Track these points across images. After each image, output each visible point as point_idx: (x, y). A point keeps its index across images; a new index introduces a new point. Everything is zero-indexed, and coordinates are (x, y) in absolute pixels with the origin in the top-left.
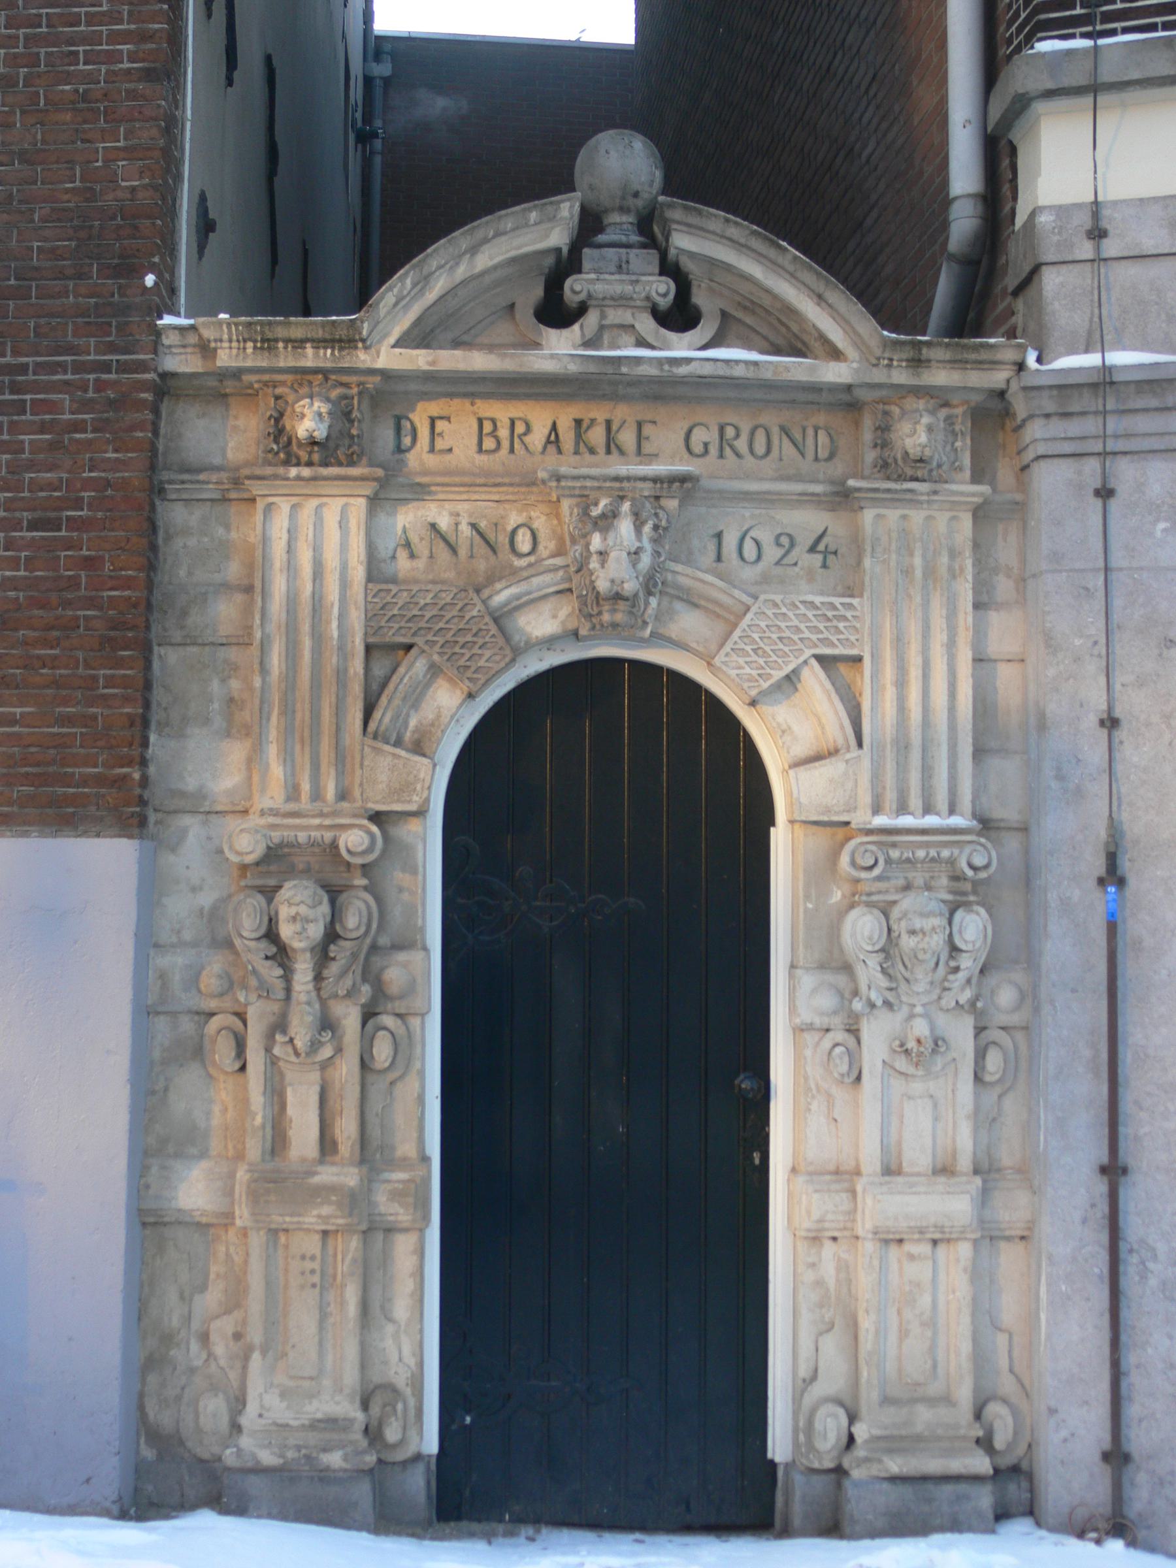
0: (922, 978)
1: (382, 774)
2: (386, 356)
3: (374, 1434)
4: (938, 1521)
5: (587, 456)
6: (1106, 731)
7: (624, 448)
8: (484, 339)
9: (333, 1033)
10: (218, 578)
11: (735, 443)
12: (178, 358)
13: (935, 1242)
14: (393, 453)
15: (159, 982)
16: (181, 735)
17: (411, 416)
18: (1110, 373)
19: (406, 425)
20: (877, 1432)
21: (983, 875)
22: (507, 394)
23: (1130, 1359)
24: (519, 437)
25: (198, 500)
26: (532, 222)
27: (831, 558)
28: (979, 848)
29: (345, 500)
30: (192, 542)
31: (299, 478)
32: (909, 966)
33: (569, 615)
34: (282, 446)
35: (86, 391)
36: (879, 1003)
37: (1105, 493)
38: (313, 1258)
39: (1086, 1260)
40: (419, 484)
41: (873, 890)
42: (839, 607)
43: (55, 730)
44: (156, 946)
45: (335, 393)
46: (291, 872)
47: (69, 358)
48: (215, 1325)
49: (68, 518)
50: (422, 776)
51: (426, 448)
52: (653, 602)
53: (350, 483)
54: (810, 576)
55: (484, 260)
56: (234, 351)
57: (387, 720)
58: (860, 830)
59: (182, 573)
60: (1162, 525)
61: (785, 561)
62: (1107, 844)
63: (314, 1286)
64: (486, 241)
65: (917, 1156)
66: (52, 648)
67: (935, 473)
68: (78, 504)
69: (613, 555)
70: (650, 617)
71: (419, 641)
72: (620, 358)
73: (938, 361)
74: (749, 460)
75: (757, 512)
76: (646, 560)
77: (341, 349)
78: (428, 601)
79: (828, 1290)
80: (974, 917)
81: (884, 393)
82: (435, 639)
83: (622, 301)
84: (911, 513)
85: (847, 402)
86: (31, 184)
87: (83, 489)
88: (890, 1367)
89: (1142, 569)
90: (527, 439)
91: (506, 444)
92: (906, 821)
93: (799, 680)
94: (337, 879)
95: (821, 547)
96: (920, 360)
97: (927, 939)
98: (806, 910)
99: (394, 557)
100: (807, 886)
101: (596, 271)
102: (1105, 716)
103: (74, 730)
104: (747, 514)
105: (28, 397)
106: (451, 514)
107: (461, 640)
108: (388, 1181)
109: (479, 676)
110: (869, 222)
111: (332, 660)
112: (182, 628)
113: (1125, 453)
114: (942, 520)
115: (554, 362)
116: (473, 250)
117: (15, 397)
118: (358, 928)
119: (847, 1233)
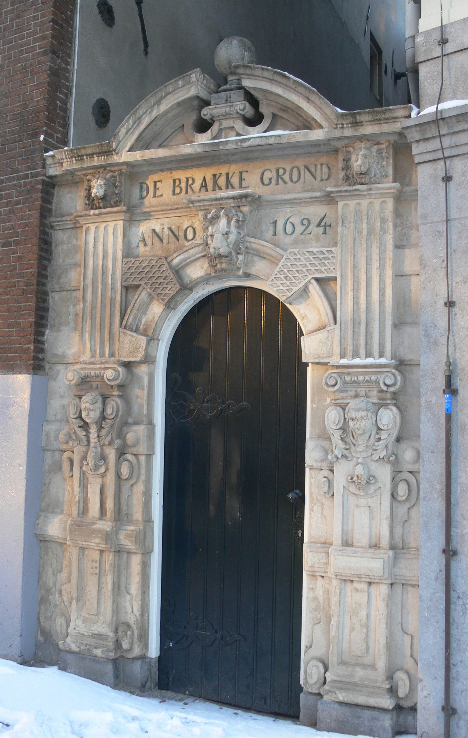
0: (361, 444)
1: (131, 345)
2: (125, 156)
3: (118, 643)
4: (363, 729)
5: (217, 191)
6: (447, 308)
7: (234, 185)
8: (172, 143)
9: (104, 461)
10: (72, 261)
11: (283, 177)
12: (54, 169)
13: (370, 583)
14: (139, 199)
15: (46, 437)
16: (59, 330)
17: (147, 182)
18: (441, 114)
19: (145, 186)
20: (335, 678)
22: (184, 167)
25: (67, 229)
26: (180, 86)
27: (328, 228)
28: (389, 374)
29: (115, 222)
30: (65, 247)
31: (94, 215)
32: (355, 437)
34: (92, 202)
35: (21, 187)
36: (339, 456)
38: (96, 562)
39: (437, 601)
40: (145, 212)
41: (340, 397)
42: (325, 252)
43: (8, 330)
44: (48, 421)
45: (108, 176)
46: (90, 389)
47: (15, 175)
48: (64, 587)
50: (142, 345)
51: (152, 196)
53: (114, 214)
54: (317, 239)
55: (164, 107)
56: (69, 163)
57: (130, 320)
58: (333, 366)
59: (61, 261)
63: (96, 574)
64: (162, 98)
65: (361, 537)
66: (7, 296)
67: (373, 179)
68: (17, 235)
70: (240, 264)
71: (142, 283)
72: (219, 142)
73: (366, 122)
74: (290, 184)
75: (293, 209)
76: (232, 237)
77: (107, 156)
78: (146, 265)
79: (319, 603)
80: (388, 411)
81: (346, 142)
82: (148, 282)
83: (227, 116)
84: (362, 201)
85: (330, 150)
86: (7, 106)
87: (19, 228)
88: (345, 646)
89: (465, 218)
90: (193, 186)
91: (184, 190)
92: (357, 361)
93: (309, 292)
94: (107, 392)
95: (323, 224)
96: (356, 123)
97: (359, 423)
99: (138, 246)
103: (13, 329)
105: (3, 193)
106: (161, 225)
107: (159, 281)
108: (126, 530)
109: (166, 298)
112: (59, 284)
113: (457, 156)
114: (377, 203)
115: (191, 148)
116: (158, 103)
118: (112, 413)
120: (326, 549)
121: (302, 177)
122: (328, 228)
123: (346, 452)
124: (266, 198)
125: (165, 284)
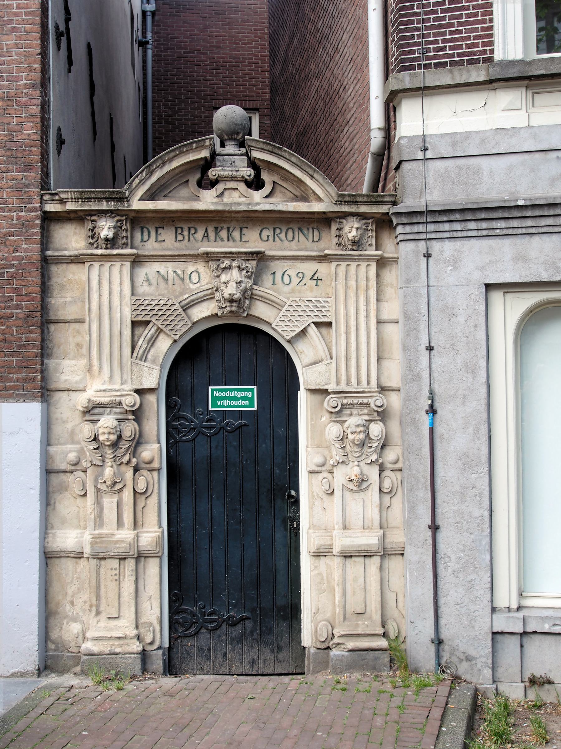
2: (137, 204)
6: (428, 351)
21: (381, 409)
23: (441, 601)
24: (192, 234)
26: (194, 147)
28: (379, 398)
37: (428, 256)
38: (116, 569)
49: (7, 272)
52: (247, 302)
54: (311, 290)
60: (450, 268)
71: (153, 319)
74: (286, 243)
75: (289, 264)
76: (243, 285)
83: (233, 179)
85: (324, 221)
90: (195, 235)
91: (187, 238)
95: (315, 277)
98: (311, 424)
100: (312, 414)
102: (428, 345)
104: (285, 264)
110: (351, 122)
120: (329, 534)
123: (344, 459)
124: (269, 253)
125: (177, 321)
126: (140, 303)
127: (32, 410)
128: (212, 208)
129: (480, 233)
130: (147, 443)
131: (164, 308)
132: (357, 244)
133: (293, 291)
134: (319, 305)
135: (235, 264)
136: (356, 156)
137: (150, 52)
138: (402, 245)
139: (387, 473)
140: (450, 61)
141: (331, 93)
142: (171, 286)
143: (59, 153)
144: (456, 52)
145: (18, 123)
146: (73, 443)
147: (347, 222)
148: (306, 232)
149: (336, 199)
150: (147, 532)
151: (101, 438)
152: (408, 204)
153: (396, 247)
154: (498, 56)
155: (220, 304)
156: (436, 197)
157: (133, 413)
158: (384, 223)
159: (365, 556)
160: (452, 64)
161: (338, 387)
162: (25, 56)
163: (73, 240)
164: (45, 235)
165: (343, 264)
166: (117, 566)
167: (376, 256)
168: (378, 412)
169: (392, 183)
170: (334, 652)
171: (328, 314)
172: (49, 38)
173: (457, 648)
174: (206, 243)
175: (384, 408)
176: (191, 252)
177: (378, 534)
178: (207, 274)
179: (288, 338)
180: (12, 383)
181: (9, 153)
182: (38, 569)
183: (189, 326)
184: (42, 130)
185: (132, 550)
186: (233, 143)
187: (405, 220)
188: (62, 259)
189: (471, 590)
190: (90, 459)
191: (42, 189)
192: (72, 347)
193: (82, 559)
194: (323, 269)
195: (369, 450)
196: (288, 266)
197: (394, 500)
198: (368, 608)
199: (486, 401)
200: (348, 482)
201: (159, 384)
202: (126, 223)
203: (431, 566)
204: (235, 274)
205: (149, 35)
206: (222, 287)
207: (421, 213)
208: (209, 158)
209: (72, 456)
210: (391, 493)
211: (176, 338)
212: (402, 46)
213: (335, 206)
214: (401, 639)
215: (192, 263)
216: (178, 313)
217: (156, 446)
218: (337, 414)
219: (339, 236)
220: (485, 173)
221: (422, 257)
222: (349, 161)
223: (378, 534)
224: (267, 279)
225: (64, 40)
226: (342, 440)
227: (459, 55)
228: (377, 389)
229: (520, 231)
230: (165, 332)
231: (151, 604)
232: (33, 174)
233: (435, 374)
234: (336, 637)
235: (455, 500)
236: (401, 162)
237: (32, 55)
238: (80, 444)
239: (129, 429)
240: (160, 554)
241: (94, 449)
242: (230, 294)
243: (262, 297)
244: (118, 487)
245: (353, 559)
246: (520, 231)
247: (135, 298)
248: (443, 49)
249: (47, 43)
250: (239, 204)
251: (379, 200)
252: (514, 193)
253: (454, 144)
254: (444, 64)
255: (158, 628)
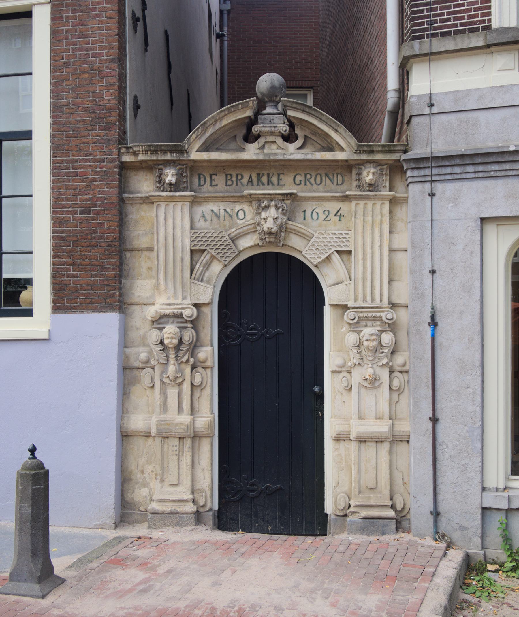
2: (194, 156)
5: (261, 186)
23: (439, 481)
24: (240, 180)
27: (342, 218)
33: (256, 239)
35: (97, 168)
38: (176, 446)
49: (93, 210)
51: (209, 185)
52: (283, 234)
60: (451, 205)
61: (326, 219)
62: (431, 312)
69: (268, 219)
71: (208, 248)
74: (315, 186)
75: (317, 203)
76: (279, 221)
83: (272, 133)
84: (368, 202)
85: (348, 167)
87: (97, 201)
90: (242, 181)
91: (235, 183)
95: (339, 214)
98: (334, 333)
101: (263, 123)
102: (431, 269)
104: (314, 203)
110: (376, 88)
111: (179, 255)
117: (74, 170)
119: (348, 439)
120: (347, 423)
121: (323, 183)
122: (342, 218)
123: (361, 361)
124: (301, 194)
126: (197, 235)
127: (112, 319)
128: (254, 157)
129: (477, 175)
130: (202, 346)
131: (217, 239)
132: (373, 187)
133: (320, 225)
134: (341, 237)
135: (273, 203)
136: (379, 116)
137: (226, 43)
138: (411, 186)
139: (396, 374)
140: (454, 30)
141: (362, 66)
142: (222, 221)
143: (136, 115)
144: (459, 22)
145: (100, 91)
146: (144, 345)
147: (365, 168)
148: (331, 177)
149: (356, 149)
150: (201, 417)
151: (166, 342)
152: (416, 152)
153: (406, 188)
154: (495, 24)
155: (261, 236)
156: (440, 147)
157: (192, 322)
158: (396, 169)
159: (376, 441)
160: (456, 32)
161: (356, 303)
162: (106, 36)
163: (145, 185)
164: (123, 181)
165: (362, 203)
166: (177, 444)
167: (389, 195)
168: (389, 324)
169: (405, 136)
170: (349, 519)
171: (348, 244)
172: (125, 22)
173: (452, 519)
174: (250, 186)
175: (394, 320)
176: (238, 194)
177: (387, 423)
178: (251, 212)
179: (315, 263)
180: (96, 298)
181: (93, 115)
182: (115, 444)
183: (236, 254)
184: (120, 96)
185: (189, 431)
186: (273, 104)
187: (413, 166)
188: (136, 200)
189: (465, 472)
190: (157, 358)
191: (119, 144)
192: (145, 270)
193: (151, 437)
194: (345, 207)
195: (381, 355)
196: (316, 205)
197: (401, 396)
198: (379, 484)
199: (479, 316)
200: (363, 381)
201: (212, 299)
202: (186, 170)
203: (432, 452)
204: (272, 212)
205: (226, 29)
206: (263, 222)
207: (426, 159)
208: (253, 117)
209: (143, 356)
210: (400, 391)
211: (226, 263)
212: (413, 19)
213: (355, 155)
214: (406, 511)
215: (239, 203)
216: (227, 243)
217: (209, 348)
218: (355, 326)
219: (359, 180)
220: (482, 125)
221: (428, 196)
222: (374, 121)
223: (387, 423)
224: (300, 216)
225: (140, 24)
226: (358, 346)
227: (462, 25)
228: (388, 305)
229: (511, 173)
230: (217, 259)
231: (204, 474)
232: (113, 132)
233: (437, 293)
234: (352, 506)
235: (452, 397)
236: (411, 117)
237: (111, 36)
238: (150, 346)
239: (188, 335)
240: (211, 435)
241: (161, 350)
242: (268, 228)
243: (294, 230)
244: (179, 380)
245: (367, 443)
246: (511, 173)
247: (193, 231)
248: (449, 20)
249: (124, 26)
250: (276, 154)
251: (392, 149)
252: (507, 141)
253: (456, 101)
254: (449, 33)
255: (209, 493)
